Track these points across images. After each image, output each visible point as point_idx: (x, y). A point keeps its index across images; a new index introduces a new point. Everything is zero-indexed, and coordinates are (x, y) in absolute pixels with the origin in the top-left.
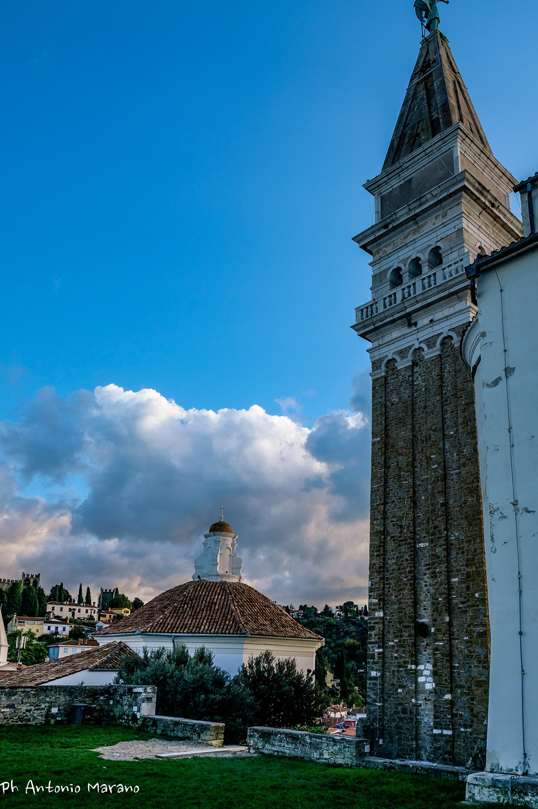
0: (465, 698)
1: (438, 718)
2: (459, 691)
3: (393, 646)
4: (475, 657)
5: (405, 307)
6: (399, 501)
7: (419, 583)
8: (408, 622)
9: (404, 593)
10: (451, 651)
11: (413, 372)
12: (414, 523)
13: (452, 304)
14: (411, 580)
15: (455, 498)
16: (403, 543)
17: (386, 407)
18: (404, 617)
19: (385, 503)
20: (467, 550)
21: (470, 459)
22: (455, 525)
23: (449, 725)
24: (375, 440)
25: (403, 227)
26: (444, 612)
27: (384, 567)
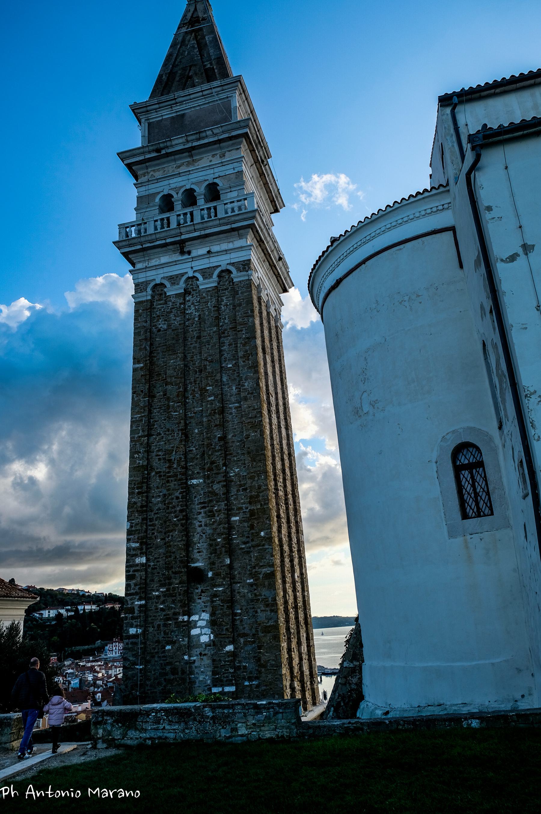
0: (249, 648)
1: (218, 674)
2: (242, 640)
3: (158, 597)
4: (262, 601)
5: (181, 233)
6: (167, 433)
7: (191, 523)
8: (179, 567)
9: (174, 535)
10: (232, 596)
11: (184, 299)
12: (185, 457)
13: (232, 240)
14: (182, 519)
15: (234, 432)
16: (172, 479)
17: (150, 332)
18: (173, 562)
19: (149, 435)
20: (250, 487)
21: (252, 393)
22: (234, 461)
23: (232, 680)
24: (137, 366)
25: (177, 157)
26: (223, 553)
27: (146, 506)
